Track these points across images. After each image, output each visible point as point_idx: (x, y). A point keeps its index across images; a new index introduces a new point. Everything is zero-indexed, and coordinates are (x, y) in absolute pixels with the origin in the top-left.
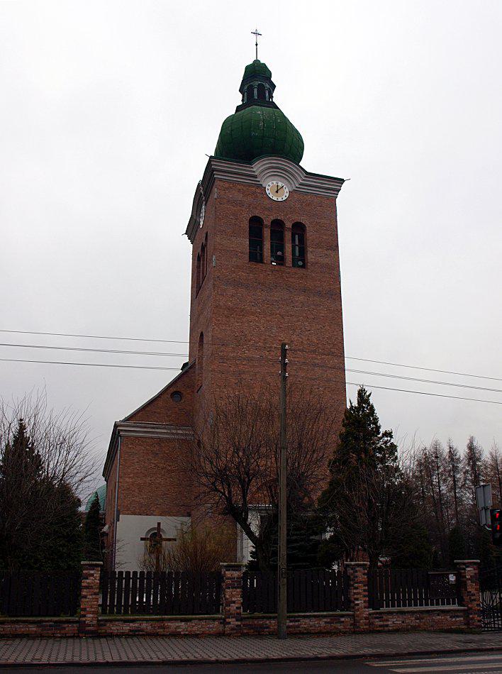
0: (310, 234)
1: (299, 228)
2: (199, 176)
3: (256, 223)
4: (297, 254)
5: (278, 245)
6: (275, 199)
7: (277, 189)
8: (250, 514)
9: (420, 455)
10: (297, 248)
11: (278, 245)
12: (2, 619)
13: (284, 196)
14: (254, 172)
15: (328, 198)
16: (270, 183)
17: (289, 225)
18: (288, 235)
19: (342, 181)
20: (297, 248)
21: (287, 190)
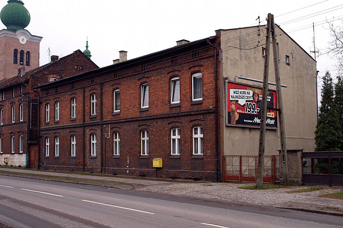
0: (32, 55)
1: (28, 53)
2: (192, 39)
3: (16, 51)
4: (27, 61)
5: (22, 60)
6: (22, 43)
7: (23, 40)
8: (303, 159)
9: (227, 128)
10: (27, 59)
11: (22, 60)
12: (342, 227)
13: (24, 43)
14: (16, 36)
15: (36, 43)
16: (21, 38)
17: (25, 52)
18: (25, 55)
19: (42, 37)
20: (27, 59)
21: (25, 40)
